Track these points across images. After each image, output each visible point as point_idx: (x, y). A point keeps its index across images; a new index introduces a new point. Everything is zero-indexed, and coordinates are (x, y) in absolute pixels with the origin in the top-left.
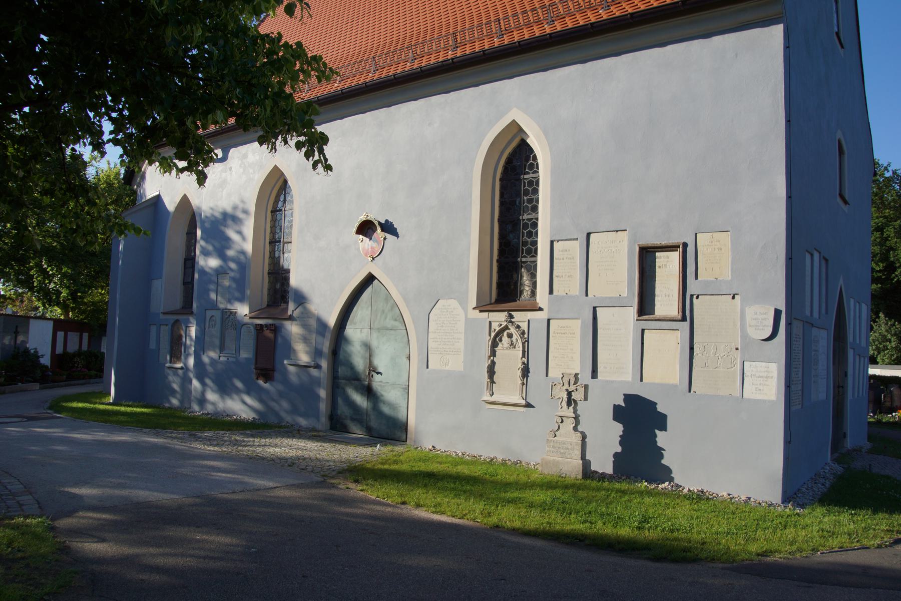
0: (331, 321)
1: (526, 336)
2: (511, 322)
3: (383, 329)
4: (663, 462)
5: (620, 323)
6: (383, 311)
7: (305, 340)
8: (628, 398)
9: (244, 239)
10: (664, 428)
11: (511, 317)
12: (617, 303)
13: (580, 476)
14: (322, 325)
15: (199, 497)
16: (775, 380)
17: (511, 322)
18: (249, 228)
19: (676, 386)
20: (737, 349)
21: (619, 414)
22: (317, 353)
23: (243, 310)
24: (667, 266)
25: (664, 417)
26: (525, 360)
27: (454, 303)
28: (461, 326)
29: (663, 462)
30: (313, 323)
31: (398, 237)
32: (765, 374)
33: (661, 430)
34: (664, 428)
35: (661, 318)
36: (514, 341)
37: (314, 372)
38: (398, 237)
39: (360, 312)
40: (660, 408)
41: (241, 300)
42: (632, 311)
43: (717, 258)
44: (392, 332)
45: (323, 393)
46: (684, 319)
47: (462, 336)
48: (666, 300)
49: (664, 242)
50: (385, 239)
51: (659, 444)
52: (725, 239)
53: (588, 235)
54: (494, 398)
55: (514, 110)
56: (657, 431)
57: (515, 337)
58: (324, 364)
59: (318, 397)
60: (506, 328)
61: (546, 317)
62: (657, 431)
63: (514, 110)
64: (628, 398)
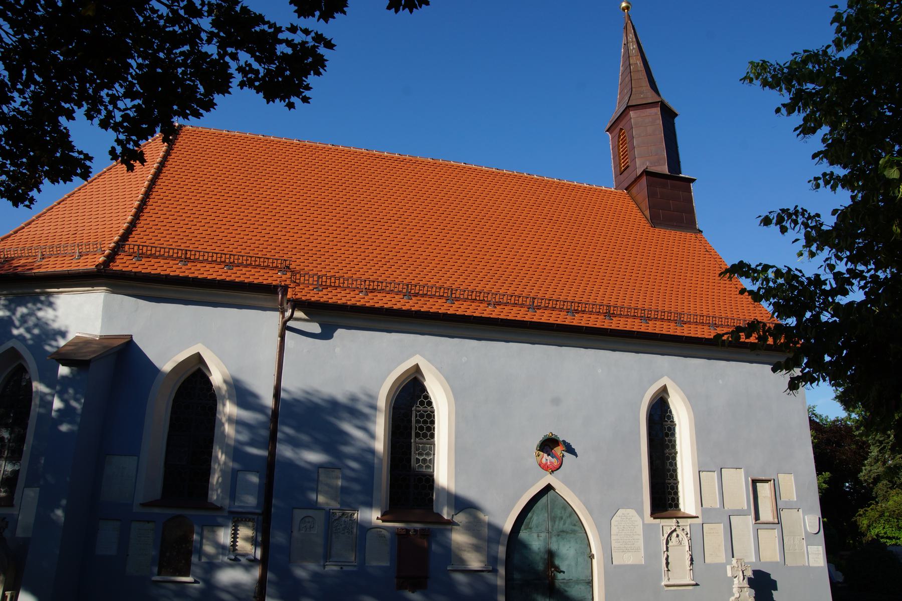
0: (508, 527)
3: (561, 534)
5: (744, 525)
6: (561, 518)
8: (755, 572)
9: (373, 436)
10: (776, 589)
12: (741, 513)
18: (380, 426)
20: (556, 401)
21: (752, 583)
22: (492, 560)
23: (374, 516)
24: (764, 490)
25: (775, 582)
27: (632, 512)
28: (640, 529)
30: (485, 531)
31: (577, 456)
34: (776, 589)
37: (489, 577)
38: (577, 456)
39: (537, 517)
40: (773, 577)
41: (370, 505)
42: (751, 518)
43: (789, 486)
44: (572, 535)
48: (767, 514)
49: (764, 478)
52: (792, 477)
58: (502, 571)
60: (675, 530)
63: (666, 377)
64: (755, 572)
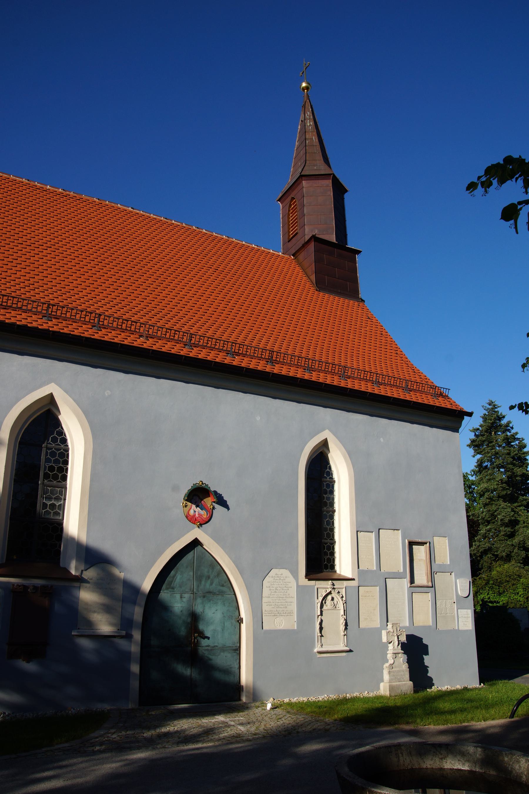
0: (147, 585)
1: (344, 599)
2: (334, 589)
4: (429, 675)
5: (399, 588)
6: (209, 577)
7: (107, 609)
10: (427, 653)
11: (333, 585)
12: (397, 576)
13: (412, 692)
14: (132, 589)
15: (443, 713)
16: (470, 619)
17: (334, 589)
19: (430, 626)
22: (125, 625)
24: (420, 552)
25: (426, 646)
26: (345, 617)
27: (285, 573)
28: (293, 591)
29: (429, 675)
30: (120, 590)
32: (466, 616)
33: (426, 655)
35: (420, 585)
36: (336, 603)
37: (122, 644)
39: (180, 576)
40: (425, 642)
42: (406, 582)
45: (135, 668)
46: (432, 587)
47: (295, 600)
50: (214, 508)
51: (426, 664)
52: (446, 540)
53: (379, 529)
54: (324, 649)
55: (327, 431)
56: (424, 656)
57: (335, 599)
58: (137, 635)
59: (128, 672)
60: (330, 593)
61: (357, 585)
62: (424, 656)
63: (327, 431)
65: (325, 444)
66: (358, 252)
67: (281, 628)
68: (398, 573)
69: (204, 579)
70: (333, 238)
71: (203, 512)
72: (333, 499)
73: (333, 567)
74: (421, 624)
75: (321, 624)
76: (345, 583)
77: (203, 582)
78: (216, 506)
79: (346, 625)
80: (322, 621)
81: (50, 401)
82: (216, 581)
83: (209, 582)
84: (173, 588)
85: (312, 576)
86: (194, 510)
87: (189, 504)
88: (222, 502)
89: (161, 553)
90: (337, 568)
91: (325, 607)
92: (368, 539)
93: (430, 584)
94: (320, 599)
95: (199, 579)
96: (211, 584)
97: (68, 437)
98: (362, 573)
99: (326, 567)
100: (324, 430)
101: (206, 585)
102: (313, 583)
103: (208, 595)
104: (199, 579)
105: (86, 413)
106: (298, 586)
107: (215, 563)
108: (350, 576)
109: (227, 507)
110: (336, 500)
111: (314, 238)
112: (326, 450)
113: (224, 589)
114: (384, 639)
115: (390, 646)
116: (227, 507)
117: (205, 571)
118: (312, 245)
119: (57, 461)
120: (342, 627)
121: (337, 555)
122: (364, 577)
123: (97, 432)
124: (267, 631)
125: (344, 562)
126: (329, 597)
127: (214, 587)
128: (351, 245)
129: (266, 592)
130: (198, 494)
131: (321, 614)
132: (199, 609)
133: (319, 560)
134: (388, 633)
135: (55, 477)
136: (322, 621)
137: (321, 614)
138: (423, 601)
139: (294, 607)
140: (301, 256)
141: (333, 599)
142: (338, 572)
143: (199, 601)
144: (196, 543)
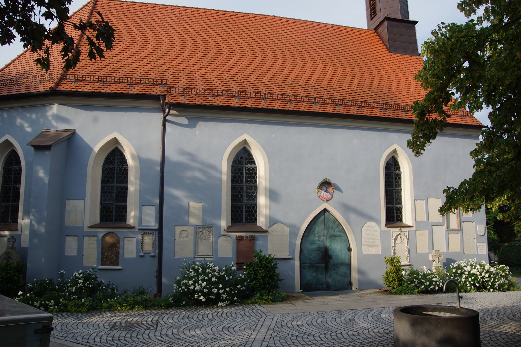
6: (332, 228)
27: (374, 224)
28: (378, 234)
39: (319, 228)
42: (444, 228)
47: (379, 239)
60: (400, 234)
65: (395, 151)
66: (417, 22)
67: (372, 253)
68: (440, 223)
69: (330, 229)
70: (399, 17)
71: (328, 194)
72: (401, 182)
73: (401, 220)
74: (454, 251)
75: (394, 250)
76: (408, 229)
77: (330, 231)
78: (335, 191)
79: (409, 251)
80: (395, 249)
81: (245, 142)
82: (337, 230)
83: (333, 230)
84: (314, 234)
85: (389, 226)
86: (323, 193)
87: (320, 190)
88: (338, 189)
89: (307, 217)
90: (404, 220)
91: (397, 242)
92: (421, 204)
93: (459, 229)
94: (394, 238)
95: (328, 229)
96: (334, 231)
97: (256, 161)
98: (417, 223)
99: (397, 220)
100: (393, 144)
101: (332, 232)
102: (389, 229)
103: (333, 237)
104: (328, 229)
105: (264, 148)
106: (381, 231)
107: (335, 220)
108: (411, 225)
109: (341, 191)
110: (402, 183)
111: (387, 19)
112: (396, 156)
113: (341, 234)
114: (431, 259)
115: (434, 263)
116: (341, 191)
117: (331, 224)
118: (385, 23)
119: (251, 173)
120: (407, 253)
121: (403, 213)
122: (420, 225)
123: (270, 157)
124: (365, 255)
125: (407, 217)
126: (399, 237)
127: (336, 233)
128: (412, 18)
129: (363, 234)
130: (326, 185)
131: (395, 246)
132: (328, 244)
133: (394, 216)
134: (432, 256)
135: (251, 181)
136: (395, 249)
137: (395, 246)
138: (455, 238)
139: (379, 242)
140: (380, 30)
141: (401, 238)
142: (404, 222)
143: (328, 240)
144: (325, 210)
